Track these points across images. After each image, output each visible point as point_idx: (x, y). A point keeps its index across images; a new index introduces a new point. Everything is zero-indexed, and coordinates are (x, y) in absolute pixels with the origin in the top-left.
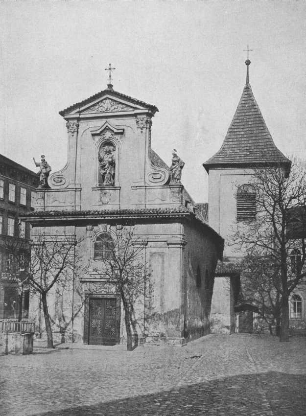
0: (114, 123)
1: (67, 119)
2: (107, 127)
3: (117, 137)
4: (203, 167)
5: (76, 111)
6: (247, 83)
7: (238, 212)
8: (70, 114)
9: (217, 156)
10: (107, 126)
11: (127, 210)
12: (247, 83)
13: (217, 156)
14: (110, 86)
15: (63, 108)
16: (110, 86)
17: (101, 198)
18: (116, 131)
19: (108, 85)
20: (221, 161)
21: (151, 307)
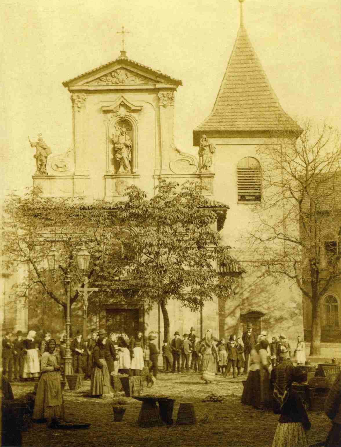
0: (131, 98)
1: (71, 91)
2: (123, 103)
3: (134, 115)
4: (192, 135)
5: (83, 82)
6: (131, 361)
7: (239, 193)
8: (77, 85)
9: (207, 122)
10: (122, 101)
11: (238, 33)
12: (131, 361)
13: (213, 116)
14: (123, 52)
15: (67, 79)
16: (123, 52)
17: (56, 281)
18: (133, 108)
19: (121, 52)
20: (215, 126)
21: (190, 335)
